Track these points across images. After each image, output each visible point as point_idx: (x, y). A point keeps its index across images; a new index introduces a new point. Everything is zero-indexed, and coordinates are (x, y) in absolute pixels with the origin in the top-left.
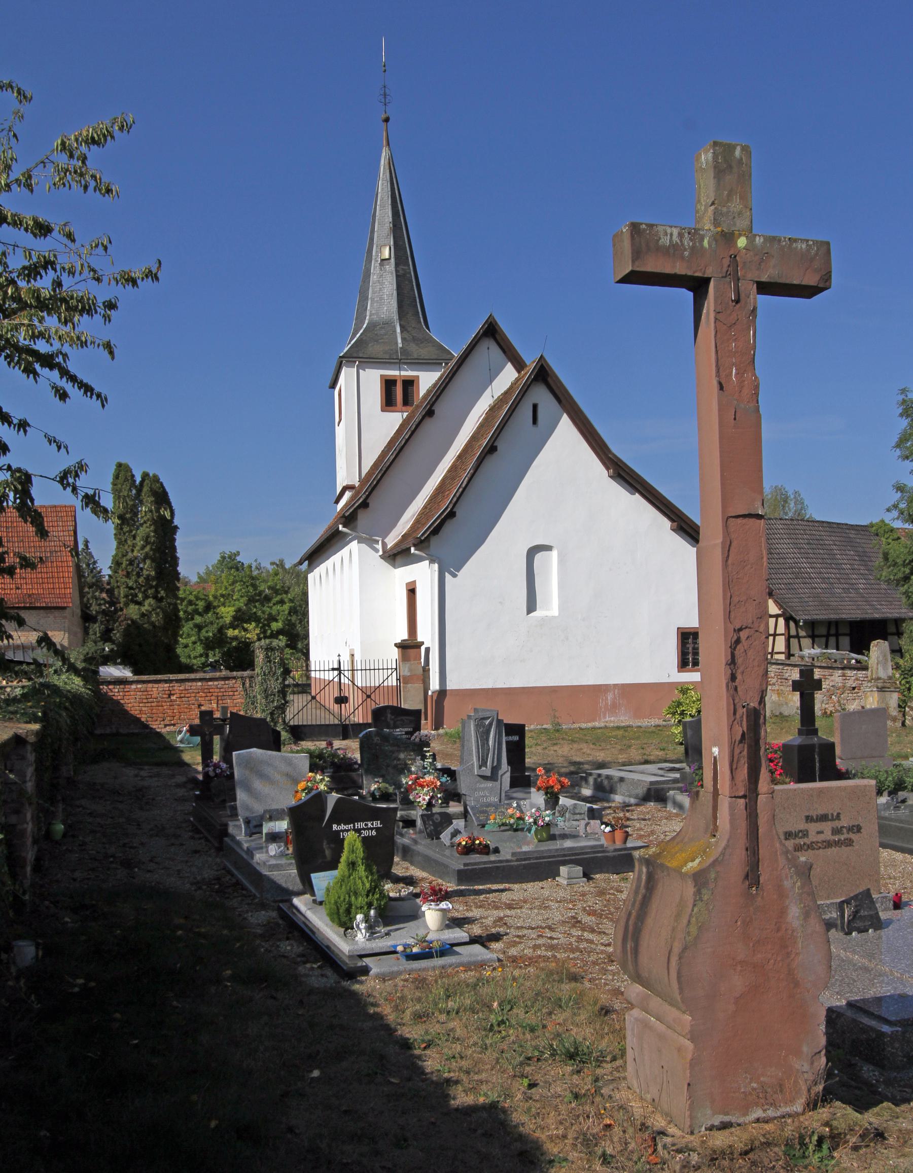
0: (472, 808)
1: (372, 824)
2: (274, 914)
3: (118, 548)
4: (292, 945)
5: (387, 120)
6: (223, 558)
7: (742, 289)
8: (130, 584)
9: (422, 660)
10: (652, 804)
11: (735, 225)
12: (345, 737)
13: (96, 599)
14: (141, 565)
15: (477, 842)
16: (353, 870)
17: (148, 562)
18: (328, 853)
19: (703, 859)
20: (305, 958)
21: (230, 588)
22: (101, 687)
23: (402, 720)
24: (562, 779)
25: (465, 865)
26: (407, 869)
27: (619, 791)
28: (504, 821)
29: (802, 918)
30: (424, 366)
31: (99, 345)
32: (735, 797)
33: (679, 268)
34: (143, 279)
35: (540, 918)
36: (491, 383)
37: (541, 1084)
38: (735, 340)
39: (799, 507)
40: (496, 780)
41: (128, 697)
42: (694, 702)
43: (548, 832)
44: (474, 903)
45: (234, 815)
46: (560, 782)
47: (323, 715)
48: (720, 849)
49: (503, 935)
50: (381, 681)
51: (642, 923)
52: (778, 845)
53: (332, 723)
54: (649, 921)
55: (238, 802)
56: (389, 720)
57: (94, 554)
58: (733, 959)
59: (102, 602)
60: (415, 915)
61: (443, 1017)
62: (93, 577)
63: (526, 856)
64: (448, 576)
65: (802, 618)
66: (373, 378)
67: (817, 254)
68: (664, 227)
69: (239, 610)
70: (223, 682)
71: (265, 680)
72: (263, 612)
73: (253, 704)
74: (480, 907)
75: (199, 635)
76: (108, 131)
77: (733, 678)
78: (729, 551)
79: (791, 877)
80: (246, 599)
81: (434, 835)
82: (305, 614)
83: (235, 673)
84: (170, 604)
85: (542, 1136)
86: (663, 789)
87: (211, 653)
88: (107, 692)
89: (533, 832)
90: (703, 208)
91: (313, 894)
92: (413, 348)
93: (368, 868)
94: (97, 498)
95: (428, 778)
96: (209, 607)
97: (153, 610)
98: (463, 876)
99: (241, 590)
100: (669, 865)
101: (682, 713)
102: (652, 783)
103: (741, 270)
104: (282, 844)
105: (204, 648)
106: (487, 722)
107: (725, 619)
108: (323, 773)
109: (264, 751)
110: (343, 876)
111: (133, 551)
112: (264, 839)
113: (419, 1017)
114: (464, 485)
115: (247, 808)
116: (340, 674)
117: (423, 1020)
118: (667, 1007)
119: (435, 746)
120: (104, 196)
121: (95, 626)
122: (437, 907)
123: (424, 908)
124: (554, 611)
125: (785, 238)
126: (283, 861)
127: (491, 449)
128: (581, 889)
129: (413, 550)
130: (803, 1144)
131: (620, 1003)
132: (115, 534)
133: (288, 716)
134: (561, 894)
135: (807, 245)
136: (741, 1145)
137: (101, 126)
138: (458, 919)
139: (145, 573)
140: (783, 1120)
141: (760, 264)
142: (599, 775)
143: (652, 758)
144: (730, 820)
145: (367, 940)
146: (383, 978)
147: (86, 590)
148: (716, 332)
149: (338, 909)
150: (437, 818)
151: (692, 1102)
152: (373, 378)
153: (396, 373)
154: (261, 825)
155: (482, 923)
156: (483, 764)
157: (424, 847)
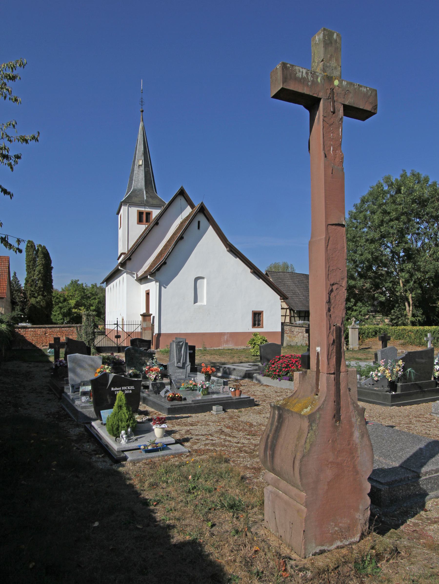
0: (174, 381)
1: (130, 388)
2: (82, 429)
3: (27, 275)
4: (90, 445)
5: (142, 111)
6: (72, 282)
7: (336, 106)
8: (32, 290)
9: (151, 321)
10: (247, 379)
11: (333, 73)
12: (119, 352)
13: (19, 296)
14: (37, 282)
15: (177, 395)
16: (120, 409)
17: (40, 281)
18: (109, 400)
19: (312, 407)
20: (96, 452)
21: (74, 293)
24: (212, 368)
25: (171, 406)
26: (145, 407)
27: (233, 374)
28: (188, 386)
29: (360, 438)
31: (6, 164)
32: (329, 374)
33: (306, 91)
34: (31, 140)
35: (206, 430)
36: (181, 213)
37: (217, 524)
38: (332, 133)
39: (292, 270)
40: (184, 369)
42: (259, 339)
43: (207, 391)
44: (176, 423)
45: (67, 383)
46: (211, 369)
47: (110, 343)
48: (321, 402)
49: (190, 439)
50: (134, 329)
51: (276, 441)
52: (349, 399)
53: (114, 346)
54: (281, 440)
55: (69, 378)
56: (137, 344)
57: (18, 278)
58: (327, 461)
59: (21, 297)
60: (150, 430)
61: (165, 485)
62: (17, 287)
63: (198, 402)
65: (296, 310)
66: (134, 211)
67: (371, 95)
68: (299, 68)
69: (77, 302)
70: (68, 329)
71: (86, 328)
72: (87, 303)
73: (81, 337)
74: (179, 425)
75: (61, 311)
76: (14, 66)
77: (329, 310)
78: (328, 242)
79: (356, 416)
80: (80, 297)
81: (157, 392)
82: (104, 304)
83: (73, 325)
84: (48, 298)
85: (222, 561)
86: (251, 373)
87: (65, 318)
89: (201, 391)
90: (316, 64)
91: (101, 420)
92: (150, 200)
93: (128, 409)
94: (7, 239)
95: (155, 367)
96: (65, 300)
97: (42, 300)
98: (171, 411)
99: (78, 293)
100: (293, 410)
101: (255, 344)
102: (247, 371)
103: (336, 97)
104: (88, 397)
105: (62, 316)
106: (181, 343)
107: (326, 279)
108: (109, 365)
109: (82, 355)
110: (116, 412)
111: (34, 276)
112: (80, 394)
113: (153, 486)
114: (170, 252)
115: (73, 380)
116: (117, 326)
117: (154, 487)
118: (290, 487)
119: (156, 356)
120: (14, 102)
121: (18, 307)
122: (160, 427)
123: (154, 427)
124: (205, 303)
125: (356, 84)
126: (88, 404)
127: (181, 238)
128: (222, 416)
129: (149, 277)
130: (363, 561)
131: (249, 474)
132: (26, 269)
133: (95, 343)
134: (214, 418)
135: (367, 90)
136: (333, 564)
137: (11, 64)
138: (169, 431)
139: (39, 285)
140: (350, 546)
141: (344, 95)
142: (225, 367)
143: (243, 361)
144: (327, 386)
145: (127, 443)
146: (134, 462)
147: (15, 292)
148: (323, 127)
149: (113, 428)
150: (159, 385)
151: (306, 541)
152: (134, 211)
154: (79, 388)
155: (180, 433)
156: (179, 361)
157: (153, 397)
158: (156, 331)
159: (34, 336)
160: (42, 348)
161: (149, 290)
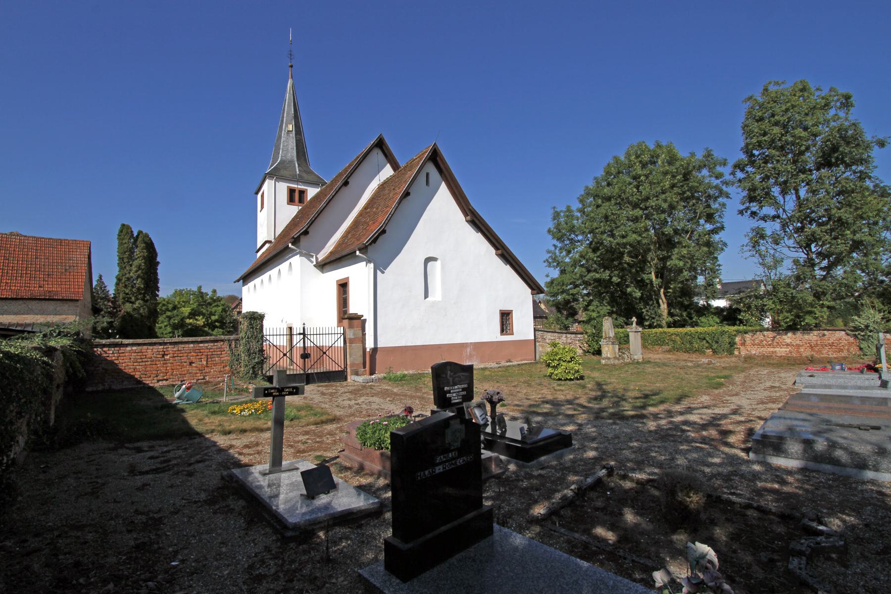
3: (119, 271)
5: (292, 66)
8: (127, 292)
17: (139, 280)
22: (95, 349)
23: (459, 377)
41: (122, 358)
50: (333, 342)
66: (283, 188)
69: (192, 310)
70: (212, 344)
71: (248, 342)
72: (207, 311)
80: (197, 303)
87: (176, 332)
88: (101, 354)
92: (304, 175)
96: (175, 308)
111: (129, 273)
129: (358, 253)
139: (137, 285)
147: (99, 300)
152: (283, 188)
153: (296, 186)
158: (370, 344)
159: (139, 360)
160: (157, 385)
161: (348, 278)
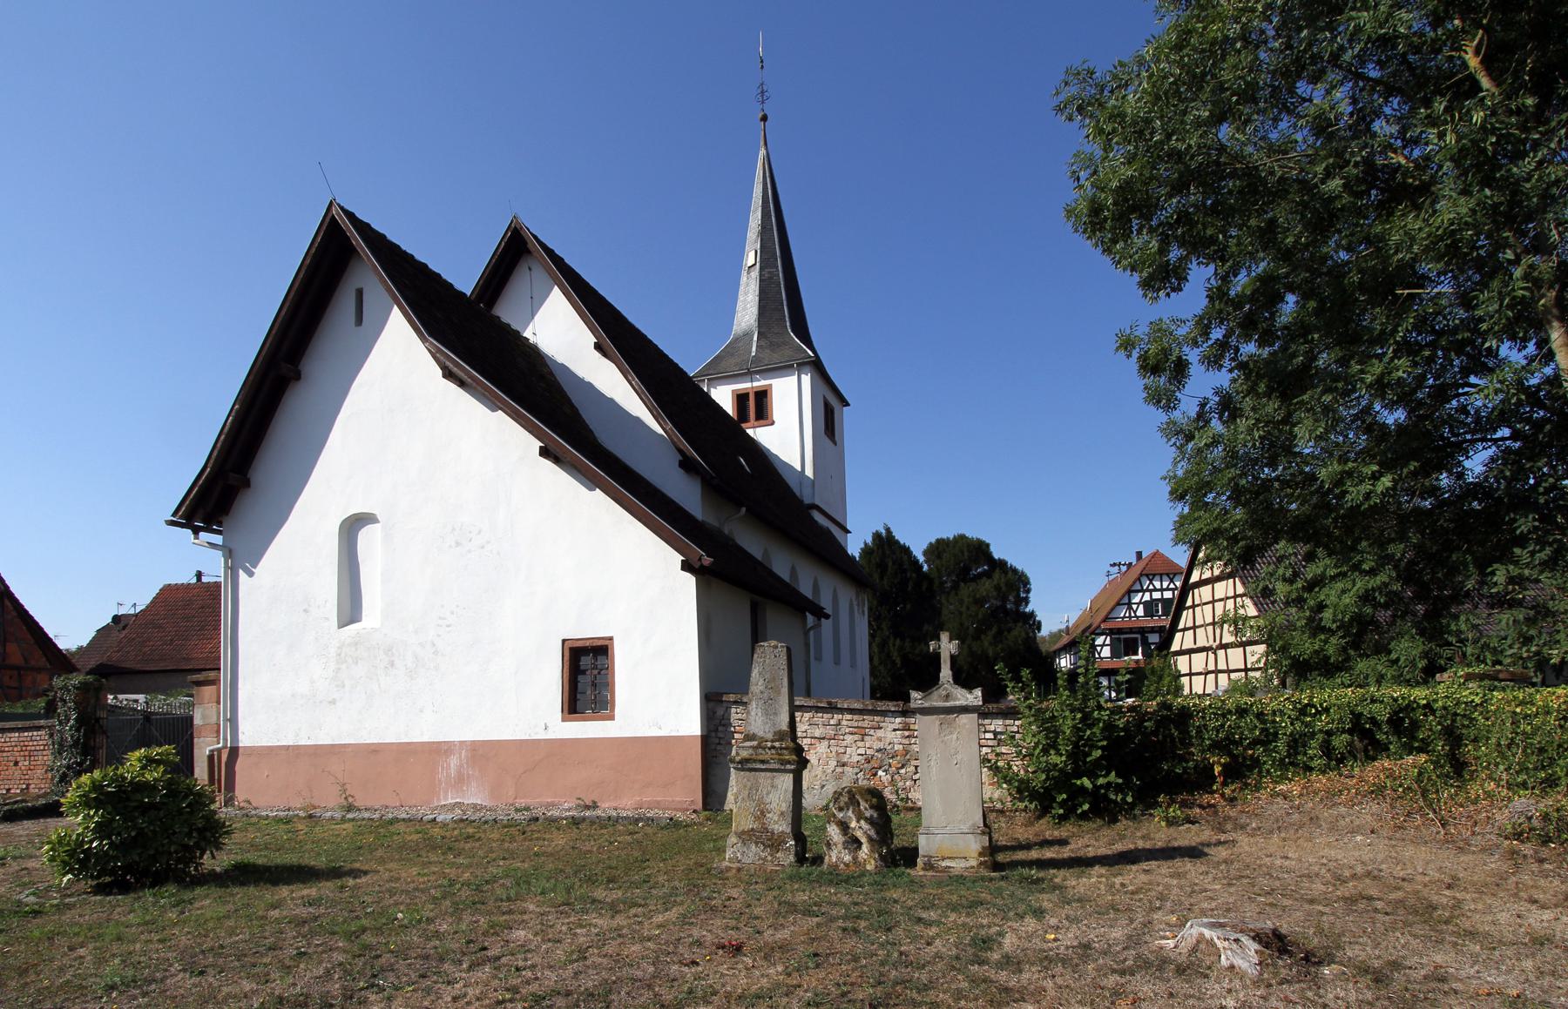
30: (778, 373)
64: (242, 575)
153: (748, 385)
